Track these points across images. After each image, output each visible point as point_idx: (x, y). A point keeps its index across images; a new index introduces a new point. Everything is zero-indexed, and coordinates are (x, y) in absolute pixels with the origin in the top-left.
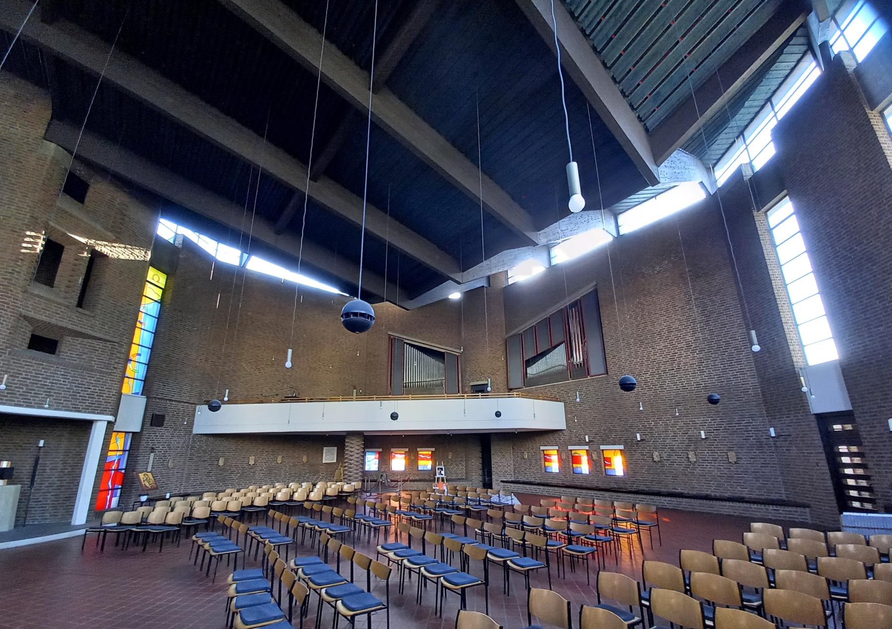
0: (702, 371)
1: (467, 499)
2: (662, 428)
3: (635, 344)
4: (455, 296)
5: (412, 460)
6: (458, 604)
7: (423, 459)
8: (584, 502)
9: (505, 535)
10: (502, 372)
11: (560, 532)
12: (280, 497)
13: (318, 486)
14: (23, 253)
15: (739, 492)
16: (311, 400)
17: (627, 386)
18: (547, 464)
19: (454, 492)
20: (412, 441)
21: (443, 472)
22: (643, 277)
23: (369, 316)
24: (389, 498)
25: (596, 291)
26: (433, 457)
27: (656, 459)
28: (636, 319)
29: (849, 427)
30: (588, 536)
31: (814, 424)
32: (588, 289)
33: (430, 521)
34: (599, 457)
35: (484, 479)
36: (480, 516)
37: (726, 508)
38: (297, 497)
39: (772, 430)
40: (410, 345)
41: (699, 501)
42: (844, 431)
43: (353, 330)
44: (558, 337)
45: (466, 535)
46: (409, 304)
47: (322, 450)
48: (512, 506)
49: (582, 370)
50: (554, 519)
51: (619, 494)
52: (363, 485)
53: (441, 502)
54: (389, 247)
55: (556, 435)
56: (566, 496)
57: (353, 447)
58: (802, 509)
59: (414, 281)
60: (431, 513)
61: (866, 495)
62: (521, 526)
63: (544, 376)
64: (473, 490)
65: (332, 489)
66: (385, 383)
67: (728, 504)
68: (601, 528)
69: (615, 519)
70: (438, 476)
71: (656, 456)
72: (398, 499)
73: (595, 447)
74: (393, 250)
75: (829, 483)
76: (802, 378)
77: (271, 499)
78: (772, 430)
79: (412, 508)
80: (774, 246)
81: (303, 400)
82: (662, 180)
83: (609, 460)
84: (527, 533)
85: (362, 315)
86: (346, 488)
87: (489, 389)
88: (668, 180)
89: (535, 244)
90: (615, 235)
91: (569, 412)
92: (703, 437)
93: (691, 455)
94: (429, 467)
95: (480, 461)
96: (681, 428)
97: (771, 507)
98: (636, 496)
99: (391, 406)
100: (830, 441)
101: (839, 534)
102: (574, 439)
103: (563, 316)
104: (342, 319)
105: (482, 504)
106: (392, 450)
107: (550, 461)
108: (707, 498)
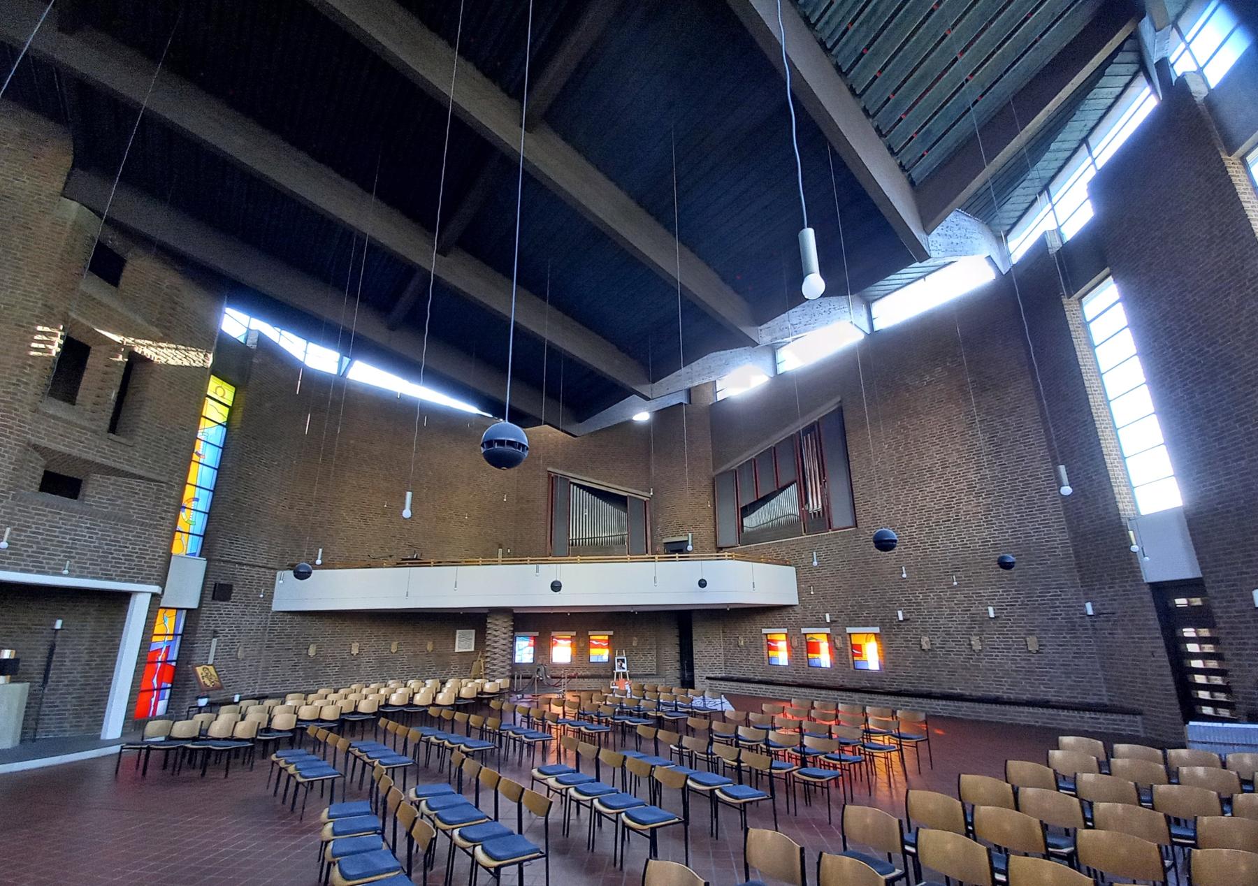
0: (990, 523)
1: (659, 703)
2: (933, 603)
3: (896, 484)
4: (642, 416)
5: (582, 648)
6: (646, 851)
7: (596, 647)
8: (824, 707)
9: (712, 754)
10: (709, 524)
11: (790, 750)
12: (394, 700)
13: (448, 685)
14: (33, 357)
15: (1042, 692)
16: (438, 564)
17: (884, 544)
18: (771, 653)
19: (640, 693)
20: (581, 622)
21: (624, 665)
22: (907, 390)
23: (521, 446)
24: (549, 702)
25: (840, 410)
26: (611, 643)
27: (925, 647)
28: (896, 449)
29: (1197, 602)
30: (830, 755)
31: (1148, 598)
32: (830, 406)
33: (607, 734)
34: (845, 644)
35: (683, 675)
36: (677, 726)
37: (1024, 716)
38: (418, 700)
39: (1089, 605)
40: (578, 485)
41: (986, 706)
42: (1190, 607)
43: (498, 465)
44: (786, 474)
45: (657, 754)
46: (577, 428)
47: (455, 634)
48: (723, 712)
49: (821, 521)
50: (781, 732)
51: (873, 696)
52: (512, 683)
53: (622, 707)
54: (549, 348)
55: (784, 613)
56: (798, 698)
57: (498, 630)
58: (1132, 717)
59: (584, 396)
60: (607, 723)
61: (1221, 697)
62: (735, 741)
63: (767, 529)
64: (666, 690)
65: (468, 689)
66: (543, 540)
67: (1026, 709)
68: (847, 744)
69: (868, 731)
70: (617, 670)
71: (925, 642)
72: (562, 703)
73: (839, 629)
74: (554, 352)
75: (1170, 681)
76: (1131, 533)
77: (382, 703)
78: (1089, 605)
79: (581, 715)
80: (1092, 347)
81: (427, 564)
82: (933, 254)
83: (859, 647)
84: (743, 751)
85: (511, 443)
86: (488, 687)
87: (690, 548)
88: (942, 254)
89: (754, 344)
90: (868, 331)
91: (803, 581)
92: (992, 615)
93: (975, 641)
94: (605, 658)
95: (678, 649)
96: (961, 603)
97: (1087, 715)
98: (897, 698)
99: (551, 571)
100: (1171, 621)
101: (1183, 752)
102: (809, 618)
103: (794, 445)
104: (483, 450)
105: (680, 709)
106: (553, 634)
107: (775, 649)
108: (997, 701)
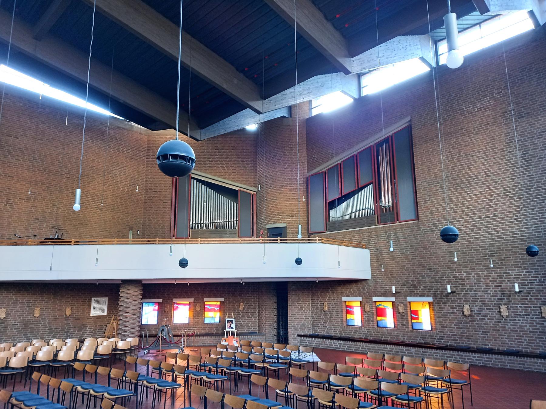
0: (519, 220)
2: (474, 280)
4: (252, 127)
5: (198, 313)
7: (210, 310)
8: (392, 359)
9: (312, 396)
12: (41, 356)
16: (77, 243)
17: (448, 237)
18: (349, 316)
19: (248, 348)
20: (198, 291)
21: (233, 325)
22: (462, 114)
25: (409, 129)
26: (222, 308)
27: (466, 313)
34: (406, 309)
35: (279, 333)
38: (61, 356)
40: (198, 180)
44: (365, 177)
45: (267, 397)
47: (90, 301)
51: (426, 350)
55: (360, 285)
57: (129, 296)
59: (207, 107)
62: (327, 386)
63: (346, 221)
65: (105, 346)
66: (172, 227)
69: (427, 378)
71: (467, 309)
73: (401, 298)
77: (31, 359)
81: (68, 243)
82: (492, 8)
83: (416, 313)
85: (183, 157)
86: (121, 345)
88: (498, 8)
89: (347, 72)
91: (376, 262)
93: (503, 309)
94: (217, 320)
96: (494, 280)
104: (158, 162)
106: (175, 300)
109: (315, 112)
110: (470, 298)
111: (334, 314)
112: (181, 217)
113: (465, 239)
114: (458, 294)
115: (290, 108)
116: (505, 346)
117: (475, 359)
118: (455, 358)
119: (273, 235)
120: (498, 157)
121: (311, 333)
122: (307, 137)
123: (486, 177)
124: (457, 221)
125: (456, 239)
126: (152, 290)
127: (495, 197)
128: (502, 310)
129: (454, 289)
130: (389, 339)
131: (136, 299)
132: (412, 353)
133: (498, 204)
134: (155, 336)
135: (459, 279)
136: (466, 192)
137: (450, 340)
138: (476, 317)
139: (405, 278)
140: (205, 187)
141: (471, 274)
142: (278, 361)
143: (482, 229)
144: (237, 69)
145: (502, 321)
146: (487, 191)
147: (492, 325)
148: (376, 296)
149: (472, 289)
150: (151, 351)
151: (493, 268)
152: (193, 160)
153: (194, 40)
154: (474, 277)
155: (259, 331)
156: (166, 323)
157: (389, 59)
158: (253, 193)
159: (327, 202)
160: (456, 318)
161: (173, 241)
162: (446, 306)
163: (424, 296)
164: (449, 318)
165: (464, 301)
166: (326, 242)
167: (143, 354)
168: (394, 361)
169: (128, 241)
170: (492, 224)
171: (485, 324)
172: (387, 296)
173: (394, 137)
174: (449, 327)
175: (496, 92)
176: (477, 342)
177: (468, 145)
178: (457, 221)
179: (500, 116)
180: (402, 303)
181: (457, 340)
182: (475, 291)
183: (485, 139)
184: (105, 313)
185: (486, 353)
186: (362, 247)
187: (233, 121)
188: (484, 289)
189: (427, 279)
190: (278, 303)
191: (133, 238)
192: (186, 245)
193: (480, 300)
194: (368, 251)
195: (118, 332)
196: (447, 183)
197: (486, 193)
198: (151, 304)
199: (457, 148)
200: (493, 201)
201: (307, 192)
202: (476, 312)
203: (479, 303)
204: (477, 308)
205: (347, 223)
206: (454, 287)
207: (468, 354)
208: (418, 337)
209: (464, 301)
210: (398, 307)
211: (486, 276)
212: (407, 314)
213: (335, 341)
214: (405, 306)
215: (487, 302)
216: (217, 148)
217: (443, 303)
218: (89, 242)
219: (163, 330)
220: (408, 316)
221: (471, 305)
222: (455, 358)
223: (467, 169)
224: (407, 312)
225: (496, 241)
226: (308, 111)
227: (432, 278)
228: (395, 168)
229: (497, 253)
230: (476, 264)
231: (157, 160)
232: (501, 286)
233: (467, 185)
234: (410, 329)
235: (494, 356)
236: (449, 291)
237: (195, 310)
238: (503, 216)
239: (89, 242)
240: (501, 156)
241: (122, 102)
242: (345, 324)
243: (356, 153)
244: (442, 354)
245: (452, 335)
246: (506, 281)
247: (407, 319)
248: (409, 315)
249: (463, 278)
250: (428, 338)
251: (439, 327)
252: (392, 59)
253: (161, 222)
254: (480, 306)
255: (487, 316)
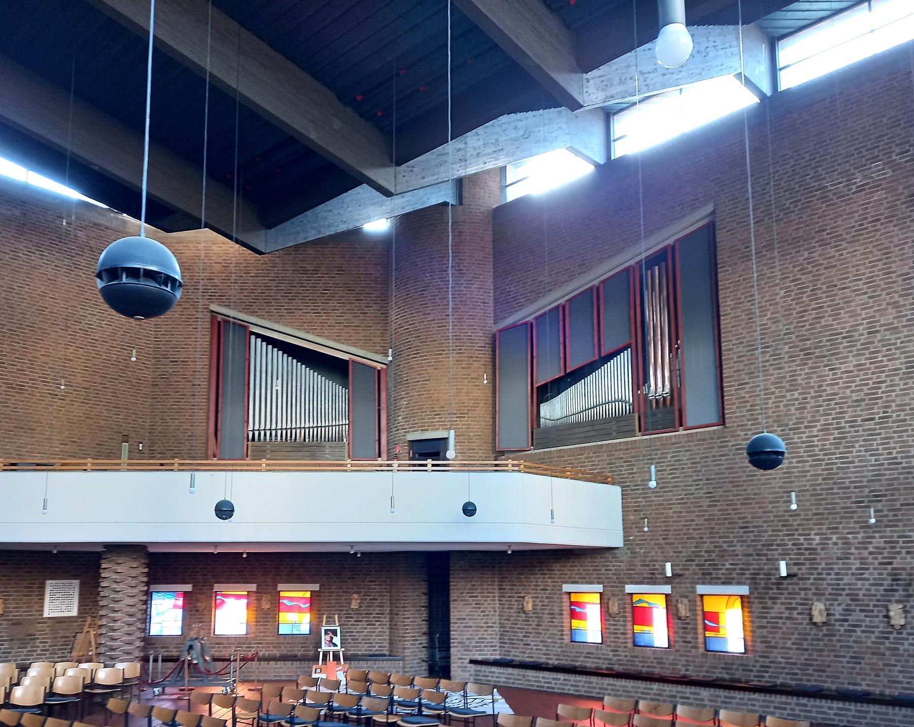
1: (392, 702)
2: (836, 551)
5: (265, 614)
7: (290, 609)
8: (655, 710)
10: (482, 413)
13: (33, 672)
17: (764, 457)
18: (576, 623)
19: (361, 685)
20: (266, 568)
21: (337, 640)
22: (823, 198)
23: (168, 280)
24: (209, 700)
25: (710, 229)
27: (818, 618)
32: (694, 221)
34: (693, 610)
35: (432, 657)
40: (265, 339)
43: (130, 314)
46: (263, 239)
47: (42, 587)
49: (666, 414)
51: (732, 693)
52: (144, 669)
53: (331, 708)
54: (213, 88)
55: (599, 560)
57: (121, 579)
63: (579, 425)
65: (68, 678)
72: (231, 702)
74: (224, 97)
77: (88, 681)
83: (714, 617)
85: (150, 274)
86: (103, 676)
87: (451, 454)
89: (575, 105)
90: (766, 89)
94: (305, 629)
96: (879, 550)
99: (215, 484)
104: (100, 284)
105: (426, 712)
106: (217, 587)
109: (512, 195)
110: (825, 589)
111: (546, 618)
112: (229, 413)
113: (821, 465)
114: (802, 579)
115: (460, 183)
116: (896, 688)
117: (832, 712)
118: (791, 709)
119: (420, 454)
120: (896, 292)
121: (498, 657)
122: (494, 248)
123: (869, 333)
124: (806, 427)
125: (779, 462)
126: (166, 565)
127: (887, 376)
128: (892, 614)
129: (795, 569)
130: (657, 671)
131: (134, 583)
132: (702, 700)
133: (893, 391)
134: (174, 660)
135: (806, 549)
136: (826, 366)
137: (781, 673)
138: (837, 628)
139: (683, 547)
140: (280, 352)
141: (830, 539)
142: (420, 711)
143: (857, 445)
144: (340, 99)
145: (891, 636)
146: (871, 363)
147: (869, 644)
148: (631, 583)
149: (832, 569)
150: (167, 690)
151: (875, 525)
152: (174, 280)
153: (245, 34)
154: (836, 544)
155: (391, 651)
156: (198, 632)
157: (667, 77)
158: (379, 366)
159: (535, 386)
160: (797, 629)
161: (214, 465)
162: (775, 603)
163: (730, 583)
164: (781, 628)
165: (814, 594)
166: (529, 470)
167: (150, 697)
168: (658, 714)
169: (119, 464)
170: (880, 434)
171: (855, 642)
172: (654, 583)
173: (677, 248)
174: (782, 648)
175: (898, 151)
176: (838, 678)
177: (835, 266)
178: (806, 427)
179: (903, 203)
180: (686, 597)
181: (796, 674)
182: (837, 574)
183: (871, 252)
184: (74, 612)
185: (856, 702)
186: (604, 482)
187: (336, 212)
188: (857, 569)
189: (738, 548)
190: (430, 595)
191: (129, 459)
192: (234, 473)
193: (847, 592)
194: (617, 490)
195: (99, 651)
196: (787, 347)
197: (869, 369)
198: (168, 595)
199: (810, 272)
200: (883, 385)
201: (494, 365)
202: (837, 617)
203: (844, 599)
204: (840, 608)
205: (577, 430)
206: (795, 564)
207: (818, 702)
208: (715, 668)
209: (814, 594)
210: (676, 606)
211: (863, 543)
212: (696, 620)
213: (547, 674)
214: (692, 602)
215: (861, 597)
216: (305, 271)
217: (770, 598)
218: (38, 465)
219: (191, 647)
220: (696, 624)
221: (828, 603)
222: (791, 709)
223: (830, 316)
224: (696, 615)
225: (886, 469)
226: (497, 192)
227: (748, 546)
228: (680, 313)
229: (885, 495)
230: (842, 518)
231: (98, 280)
232: (891, 563)
233: (828, 350)
234: (701, 650)
235: (873, 708)
236: (784, 573)
237: (259, 608)
238: (902, 417)
239: (38, 465)
240: (903, 290)
241: (97, 168)
242: (567, 639)
243: (596, 282)
244: (764, 701)
245: (787, 663)
246: (904, 555)
247: (696, 629)
248: (700, 621)
249: (814, 546)
250: (737, 670)
251: (760, 647)
252: (675, 76)
253: (187, 426)
254: (848, 605)
255: (860, 626)
